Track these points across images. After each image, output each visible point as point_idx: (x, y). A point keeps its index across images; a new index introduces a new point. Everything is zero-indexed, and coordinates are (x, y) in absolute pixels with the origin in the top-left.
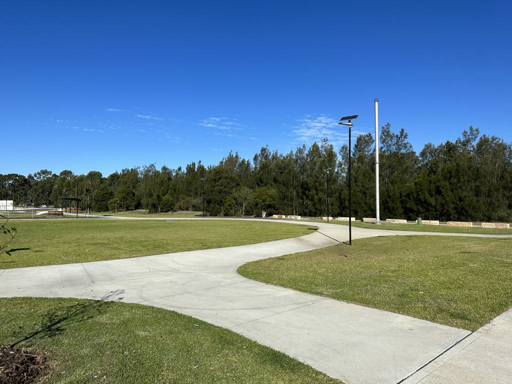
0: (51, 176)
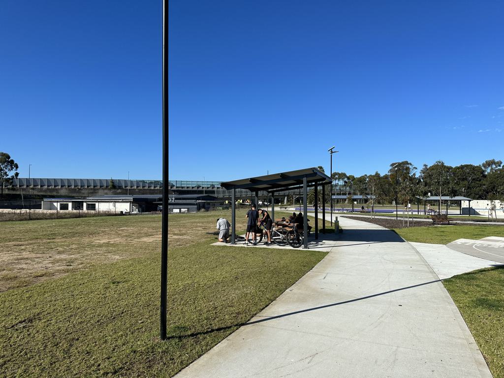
0: (501, 168)
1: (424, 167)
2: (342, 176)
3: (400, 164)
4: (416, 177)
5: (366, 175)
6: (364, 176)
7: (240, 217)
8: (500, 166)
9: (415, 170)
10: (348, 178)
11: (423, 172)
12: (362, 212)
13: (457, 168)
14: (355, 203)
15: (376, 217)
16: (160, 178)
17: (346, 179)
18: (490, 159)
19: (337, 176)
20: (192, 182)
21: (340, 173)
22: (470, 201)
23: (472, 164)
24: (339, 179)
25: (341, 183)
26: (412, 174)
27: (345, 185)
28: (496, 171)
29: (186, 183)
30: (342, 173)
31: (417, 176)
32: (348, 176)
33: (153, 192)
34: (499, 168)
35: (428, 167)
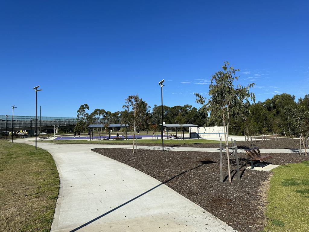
0: (192, 109)
1: (155, 107)
2: (102, 112)
4: (150, 113)
5: (119, 111)
6: (117, 112)
7: (9, 155)
8: (191, 108)
9: (149, 109)
10: (107, 113)
11: (154, 110)
12: (117, 139)
13: (173, 108)
14: (111, 131)
16: (161, 105)
20: (22, 116)
21: (101, 109)
22: (198, 127)
23: (180, 106)
24: (100, 114)
25: (101, 117)
26: (148, 111)
27: (104, 119)
28: (189, 110)
29: (25, 118)
30: (102, 110)
31: (150, 112)
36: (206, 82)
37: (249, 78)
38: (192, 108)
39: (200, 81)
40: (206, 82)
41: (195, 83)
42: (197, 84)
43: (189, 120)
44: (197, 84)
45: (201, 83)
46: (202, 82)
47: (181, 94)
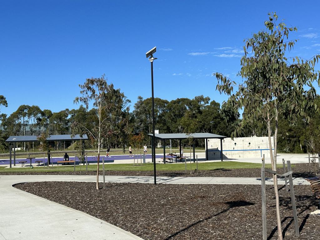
0: (209, 104)
1: (139, 100)
2: (33, 111)
3: (209, 98)
6: (65, 111)
8: (208, 103)
9: (128, 104)
10: (43, 114)
13: (174, 102)
15: (110, 179)
17: (39, 115)
18: (199, 95)
19: (26, 111)
21: (31, 106)
24: (30, 115)
25: (32, 121)
26: (125, 109)
27: (38, 124)
28: (205, 107)
30: (34, 107)
31: (131, 111)
32: (43, 110)
33: (270, 141)
34: (207, 104)
35: (143, 100)
36: (236, 54)
37: (316, 45)
38: (210, 102)
39: (225, 52)
40: (236, 54)
41: (214, 54)
42: (218, 56)
43: (204, 126)
44: (218, 56)
45: (226, 56)
46: (229, 54)
47: (190, 75)
